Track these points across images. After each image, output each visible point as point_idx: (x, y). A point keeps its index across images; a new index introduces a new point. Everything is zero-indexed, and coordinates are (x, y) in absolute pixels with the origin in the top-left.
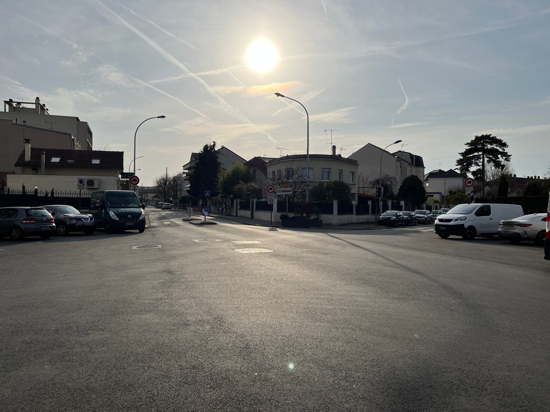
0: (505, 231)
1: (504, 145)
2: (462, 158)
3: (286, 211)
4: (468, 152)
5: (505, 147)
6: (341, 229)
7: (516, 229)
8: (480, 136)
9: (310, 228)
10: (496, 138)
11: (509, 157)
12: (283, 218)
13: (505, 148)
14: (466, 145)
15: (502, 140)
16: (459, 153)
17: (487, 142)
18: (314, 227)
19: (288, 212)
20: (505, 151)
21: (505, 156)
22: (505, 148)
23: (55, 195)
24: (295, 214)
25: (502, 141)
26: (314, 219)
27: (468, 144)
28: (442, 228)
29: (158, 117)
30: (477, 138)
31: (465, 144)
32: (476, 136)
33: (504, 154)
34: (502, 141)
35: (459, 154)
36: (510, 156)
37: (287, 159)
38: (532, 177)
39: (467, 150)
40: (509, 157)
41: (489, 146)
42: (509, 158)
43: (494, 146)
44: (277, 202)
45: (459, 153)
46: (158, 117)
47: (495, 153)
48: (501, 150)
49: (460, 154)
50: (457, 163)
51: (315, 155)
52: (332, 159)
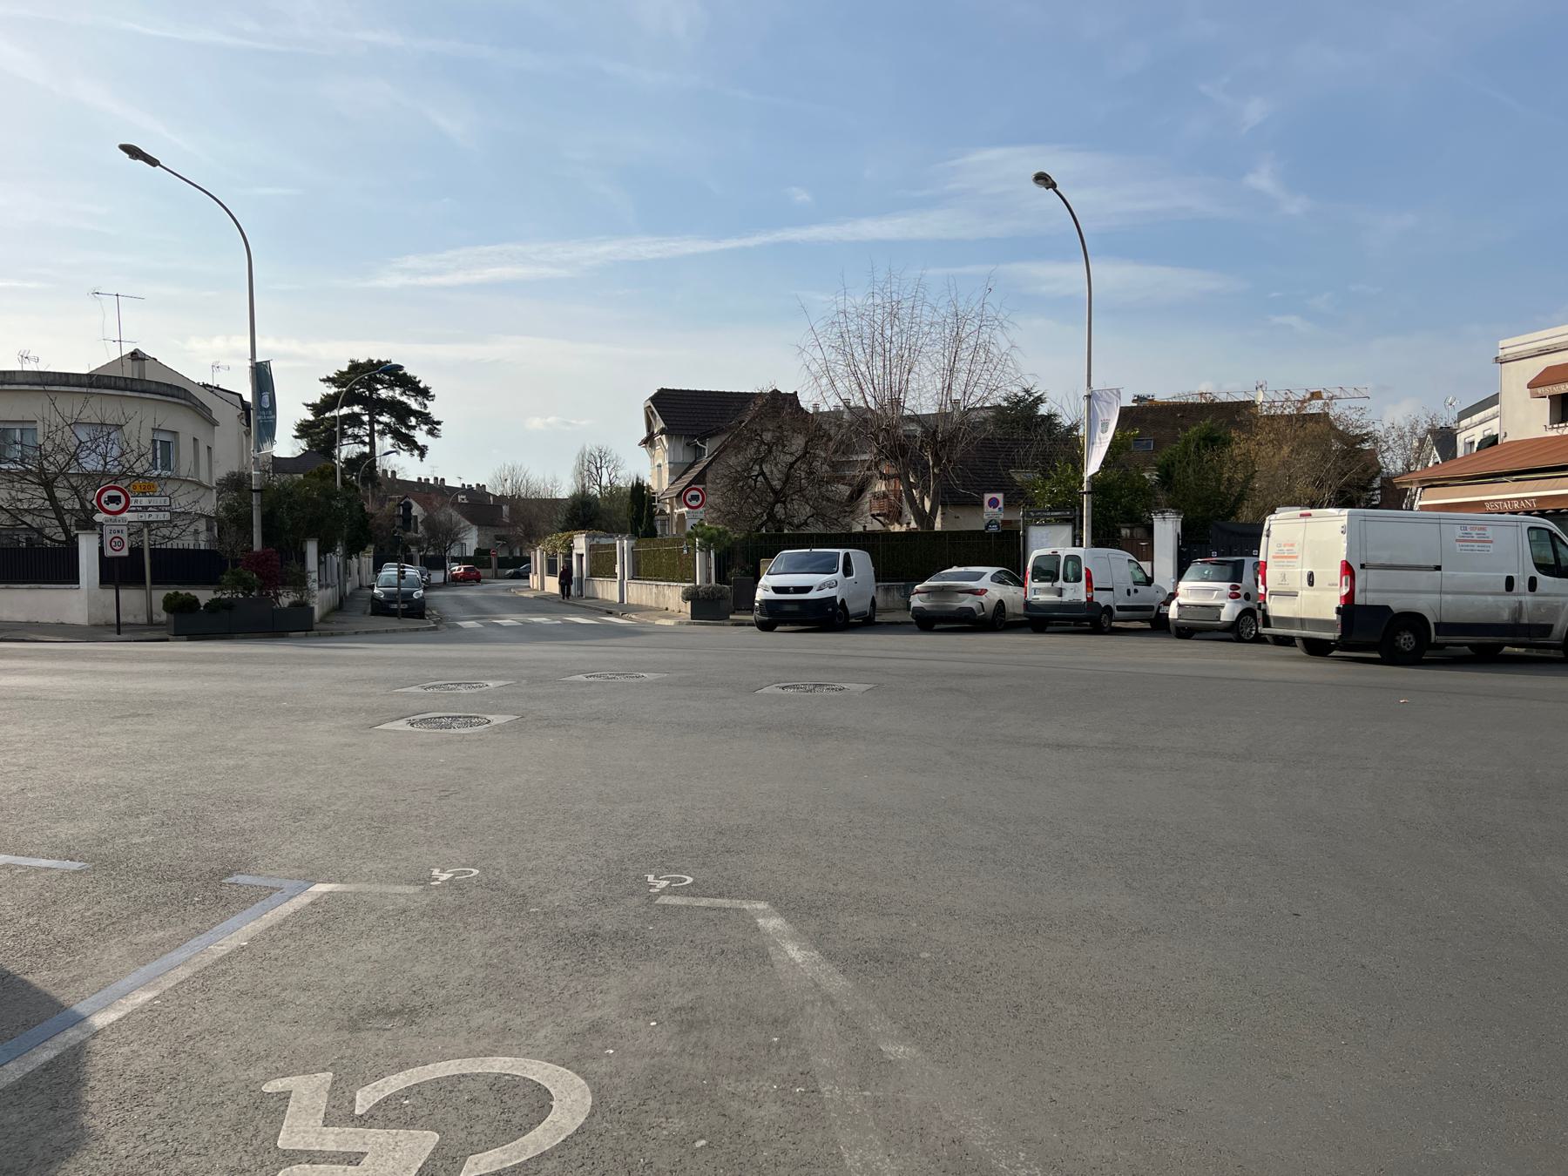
0: (937, 606)
1: (425, 393)
2: (311, 418)
3: (144, 583)
4: (329, 403)
5: (428, 399)
6: (417, 630)
7: (964, 600)
8: (783, 392)
9: (288, 636)
10: (405, 374)
11: (437, 427)
12: (171, 605)
13: (426, 402)
14: (322, 383)
15: (417, 380)
16: (305, 404)
17: (381, 382)
18: (304, 633)
19: (153, 582)
20: (427, 411)
21: (426, 424)
22: (426, 402)
23: (867, 529)
24: (215, 593)
25: (420, 381)
26: (293, 605)
27: (328, 380)
28: (788, 608)
29: (153, 162)
30: (355, 367)
31: (321, 380)
32: (352, 361)
33: (425, 418)
34: (420, 381)
35: (305, 407)
36: (439, 423)
37: (91, 386)
38: (428, 480)
39: (328, 396)
40: (437, 427)
41: (384, 393)
42: (436, 428)
43: (397, 393)
44: (1096, 547)
45: (305, 404)
46: (153, 162)
47: (402, 412)
48: (415, 406)
49: (308, 405)
50: (297, 430)
51: (54, 373)
52: (167, 395)
